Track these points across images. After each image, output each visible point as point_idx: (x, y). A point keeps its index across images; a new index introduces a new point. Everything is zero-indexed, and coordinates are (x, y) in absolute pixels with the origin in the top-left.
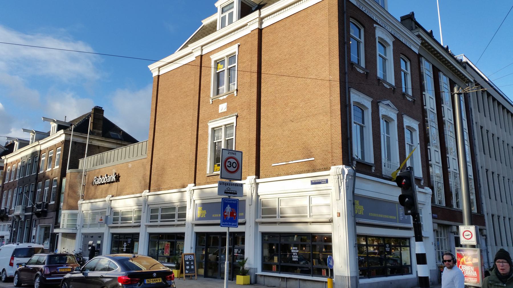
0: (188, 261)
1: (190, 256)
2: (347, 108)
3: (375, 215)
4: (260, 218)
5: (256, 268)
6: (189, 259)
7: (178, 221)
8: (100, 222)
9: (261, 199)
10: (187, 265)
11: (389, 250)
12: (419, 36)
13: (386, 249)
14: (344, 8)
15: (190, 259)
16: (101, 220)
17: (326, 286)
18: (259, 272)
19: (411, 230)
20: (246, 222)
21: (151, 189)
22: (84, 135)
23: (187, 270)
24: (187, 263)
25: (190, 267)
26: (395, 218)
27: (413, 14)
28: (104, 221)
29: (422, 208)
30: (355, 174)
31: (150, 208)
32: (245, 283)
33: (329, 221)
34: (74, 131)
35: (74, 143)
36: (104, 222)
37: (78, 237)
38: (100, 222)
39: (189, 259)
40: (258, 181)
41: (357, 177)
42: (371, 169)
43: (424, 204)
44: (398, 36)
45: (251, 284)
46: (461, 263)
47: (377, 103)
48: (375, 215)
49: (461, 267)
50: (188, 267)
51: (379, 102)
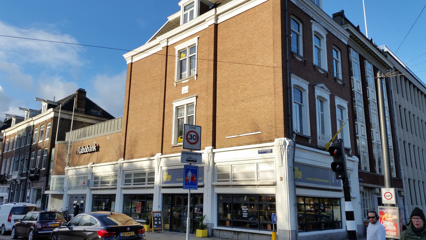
0: (156, 217)
1: (158, 213)
2: (288, 90)
3: (311, 179)
4: (216, 182)
5: (213, 223)
6: (157, 216)
7: (148, 184)
8: (83, 185)
9: (216, 166)
10: (156, 221)
11: (323, 209)
12: (348, 30)
13: (321, 207)
15: (158, 216)
16: (84, 183)
17: (271, 238)
18: (215, 227)
19: (341, 192)
20: (204, 185)
21: (126, 157)
22: (69, 112)
23: (156, 225)
24: (156, 219)
25: (158, 223)
26: (328, 181)
27: (343, 11)
28: (86, 184)
29: (351, 173)
30: (295, 145)
31: (125, 173)
32: (204, 236)
33: (273, 184)
34: (61, 109)
35: (62, 119)
36: (86, 185)
37: (65, 197)
38: (83, 185)
39: (157, 216)
40: (214, 151)
41: (297, 147)
42: (308, 141)
43: (352, 170)
44: (331, 30)
45: (208, 236)
46: (383, 219)
47: (313, 86)
48: (311, 179)
49: (383, 222)
50: (156, 223)
51: (315, 85)
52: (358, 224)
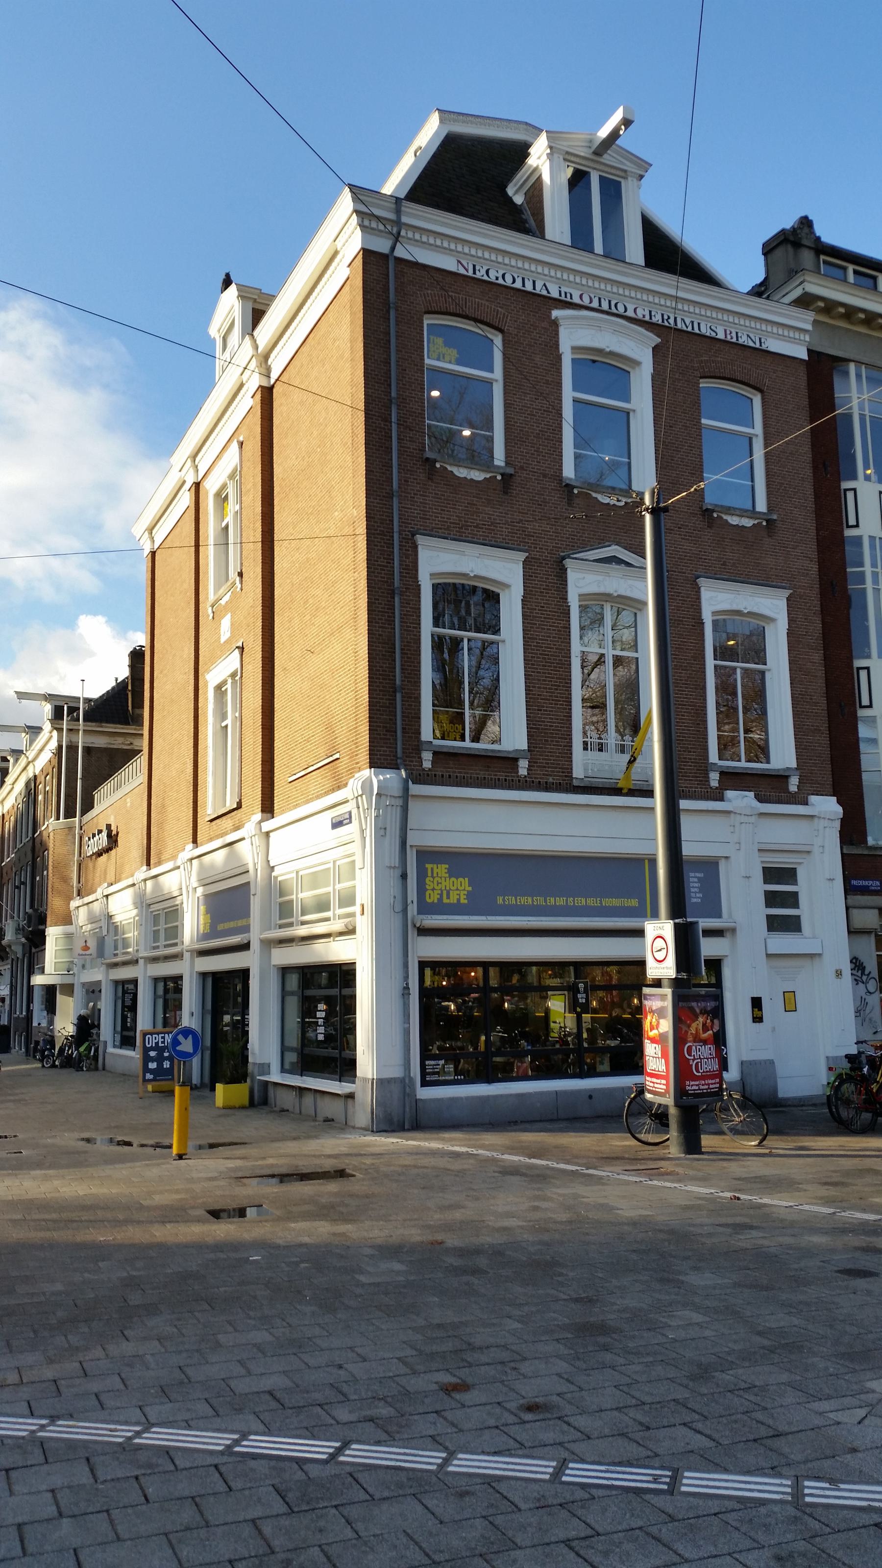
0: (156, 1048)
1: (161, 1036)
2: (394, 598)
3: (512, 900)
4: (275, 929)
5: (267, 1062)
6: (157, 1043)
7: (166, 946)
8: (84, 953)
9: (276, 878)
10: (152, 1060)
11: (584, 1001)
12: (805, 301)
13: (579, 996)
14: (386, 289)
15: (160, 1045)
16: (86, 948)
17: (790, 1103)
18: (275, 1076)
19: (723, 936)
20: (249, 943)
21: (152, 862)
22: (106, 727)
23: (151, 1071)
24: (152, 1054)
25: (160, 1065)
26: (634, 903)
27: (806, 223)
28: (93, 949)
29: (800, 863)
30: (406, 789)
31: (152, 912)
32: (232, 1104)
33: (344, 929)
34: (85, 720)
35: (88, 750)
36: (95, 955)
37: (78, 990)
38: (84, 953)
39: (157, 1043)
40: (267, 826)
41: (413, 796)
42: (516, 768)
43: (809, 852)
44: (688, 321)
45: (252, 1104)
46: (690, 1038)
47: (561, 562)
48: (512, 900)
49: (690, 1048)
50: (153, 1065)
51: (564, 558)
52: (830, 1055)
